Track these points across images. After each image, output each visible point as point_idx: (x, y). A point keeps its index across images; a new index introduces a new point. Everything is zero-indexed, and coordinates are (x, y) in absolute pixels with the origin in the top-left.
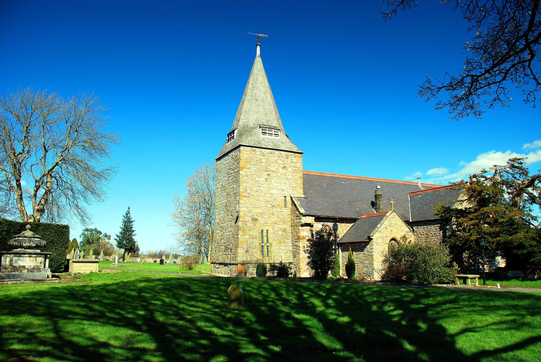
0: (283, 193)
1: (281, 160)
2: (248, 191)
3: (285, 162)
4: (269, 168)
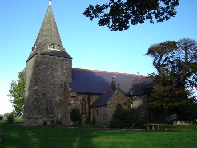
0: (61, 80)
1: (59, 62)
2: (41, 79)
3: (62, 63)
4: (53, 66)
